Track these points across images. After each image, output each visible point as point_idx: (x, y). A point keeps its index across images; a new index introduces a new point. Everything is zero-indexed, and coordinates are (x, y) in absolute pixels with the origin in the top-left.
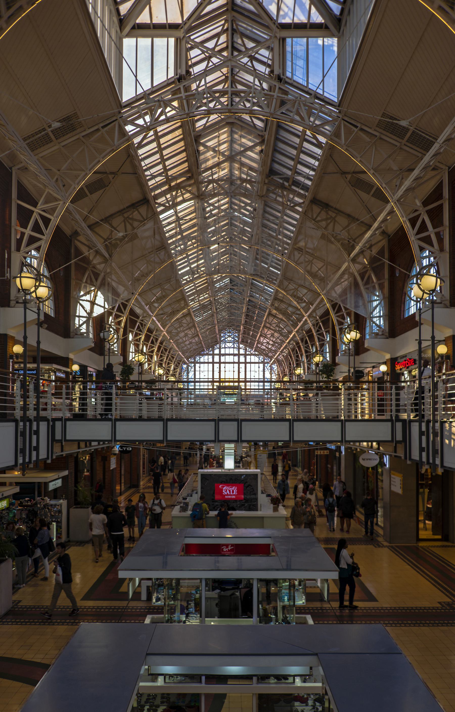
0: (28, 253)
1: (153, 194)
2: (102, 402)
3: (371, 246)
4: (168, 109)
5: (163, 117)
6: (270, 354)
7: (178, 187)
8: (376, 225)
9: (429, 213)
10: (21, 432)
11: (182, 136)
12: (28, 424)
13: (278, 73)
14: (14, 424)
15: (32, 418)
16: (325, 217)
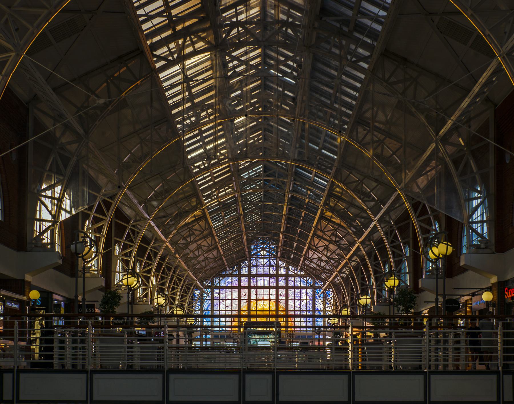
1: (149, 42)
6: (323, 276)
7: (186, 33)
8: (476, 89)
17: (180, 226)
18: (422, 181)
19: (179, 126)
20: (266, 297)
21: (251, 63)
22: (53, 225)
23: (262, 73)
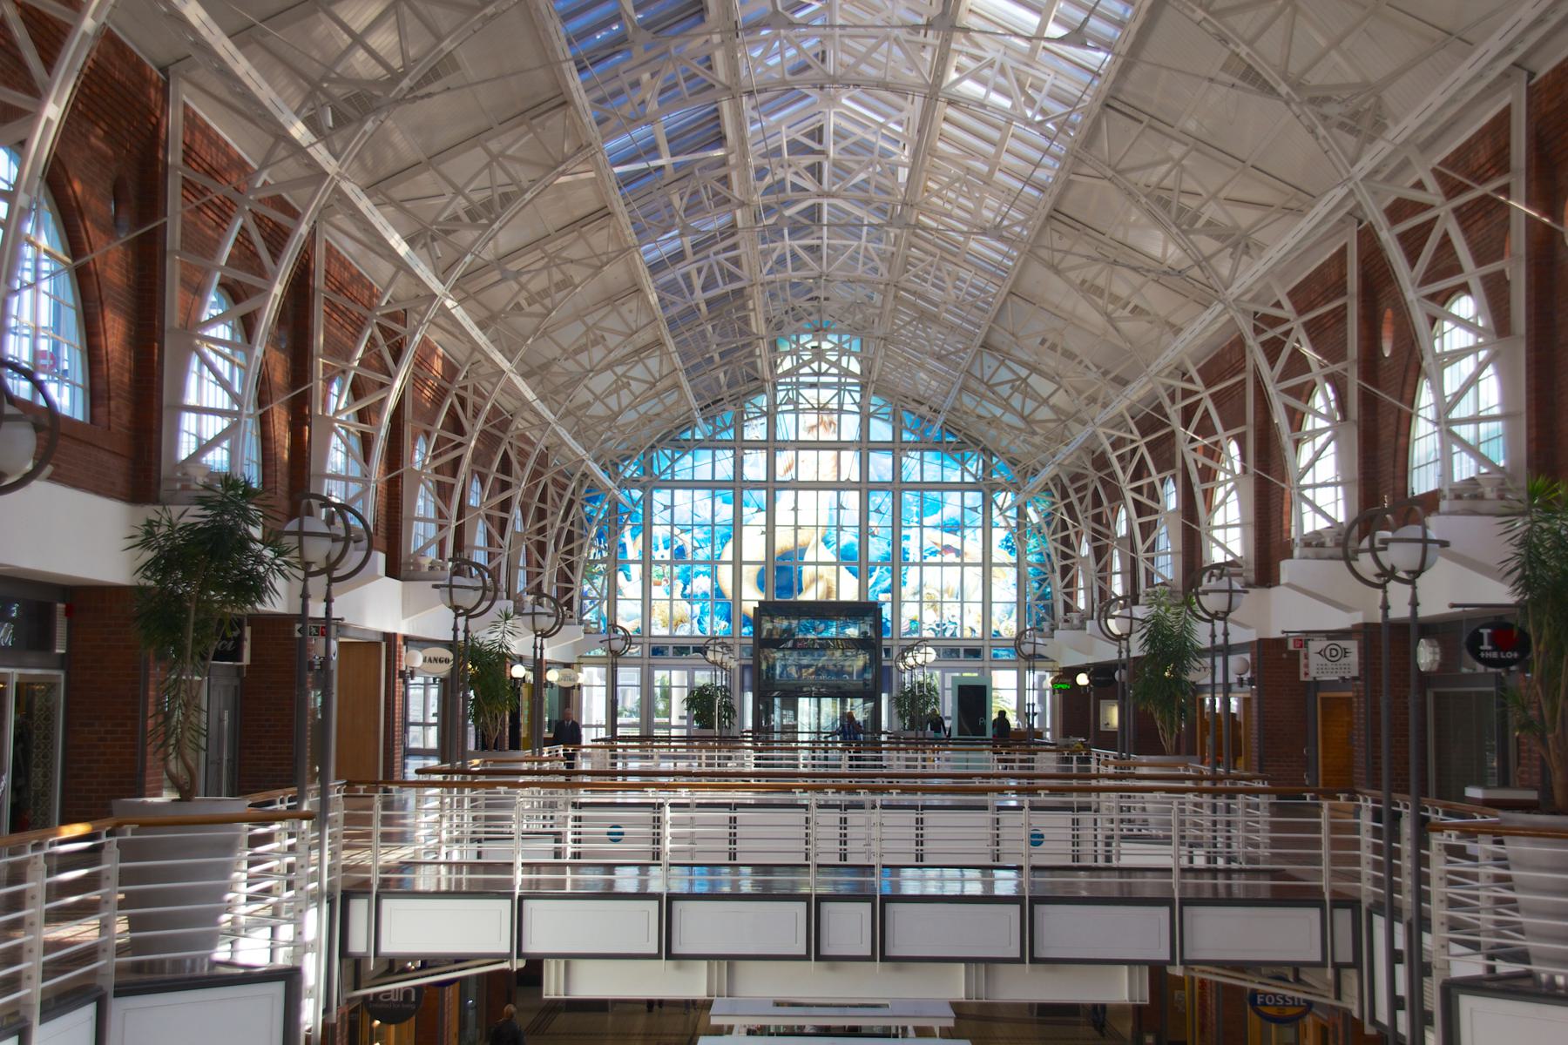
2: (337, 813)
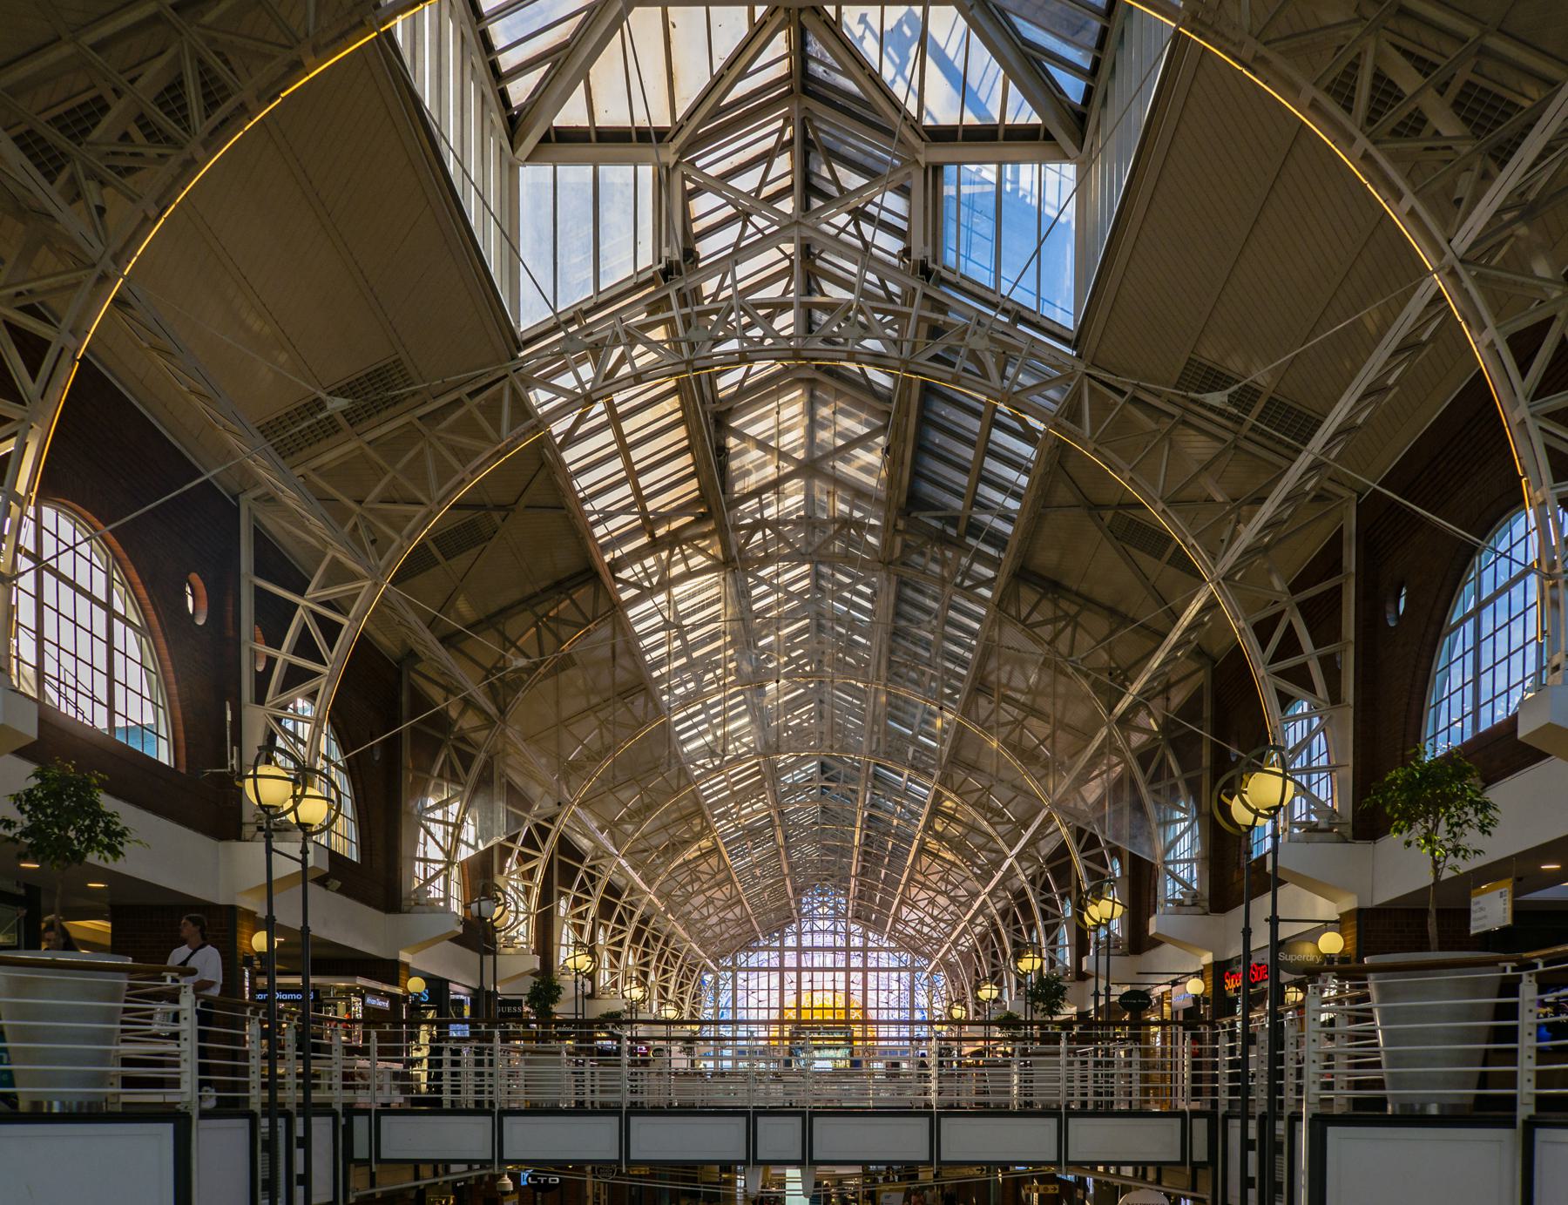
0: (285, 708)
1: (607, 558)
3: (1168, 687)
4: (640, 349)
5: (625, 369)
6: (927, 949)
7: (674, 540)
8: (1174, 636)
9: (1305, 609)
10: (263, 1141)
11: (679, 414)
12: (281, 1122)
13: (921, 257)
14: (245, 1123)
15: (291, 1107)
16: (1050, 615)
17: (673, 866)
18: (1093, 791)
19: (665, 698)
20: (829, 986)
21: (791, 589)
22: (446, 868)
23: (813, 604)
